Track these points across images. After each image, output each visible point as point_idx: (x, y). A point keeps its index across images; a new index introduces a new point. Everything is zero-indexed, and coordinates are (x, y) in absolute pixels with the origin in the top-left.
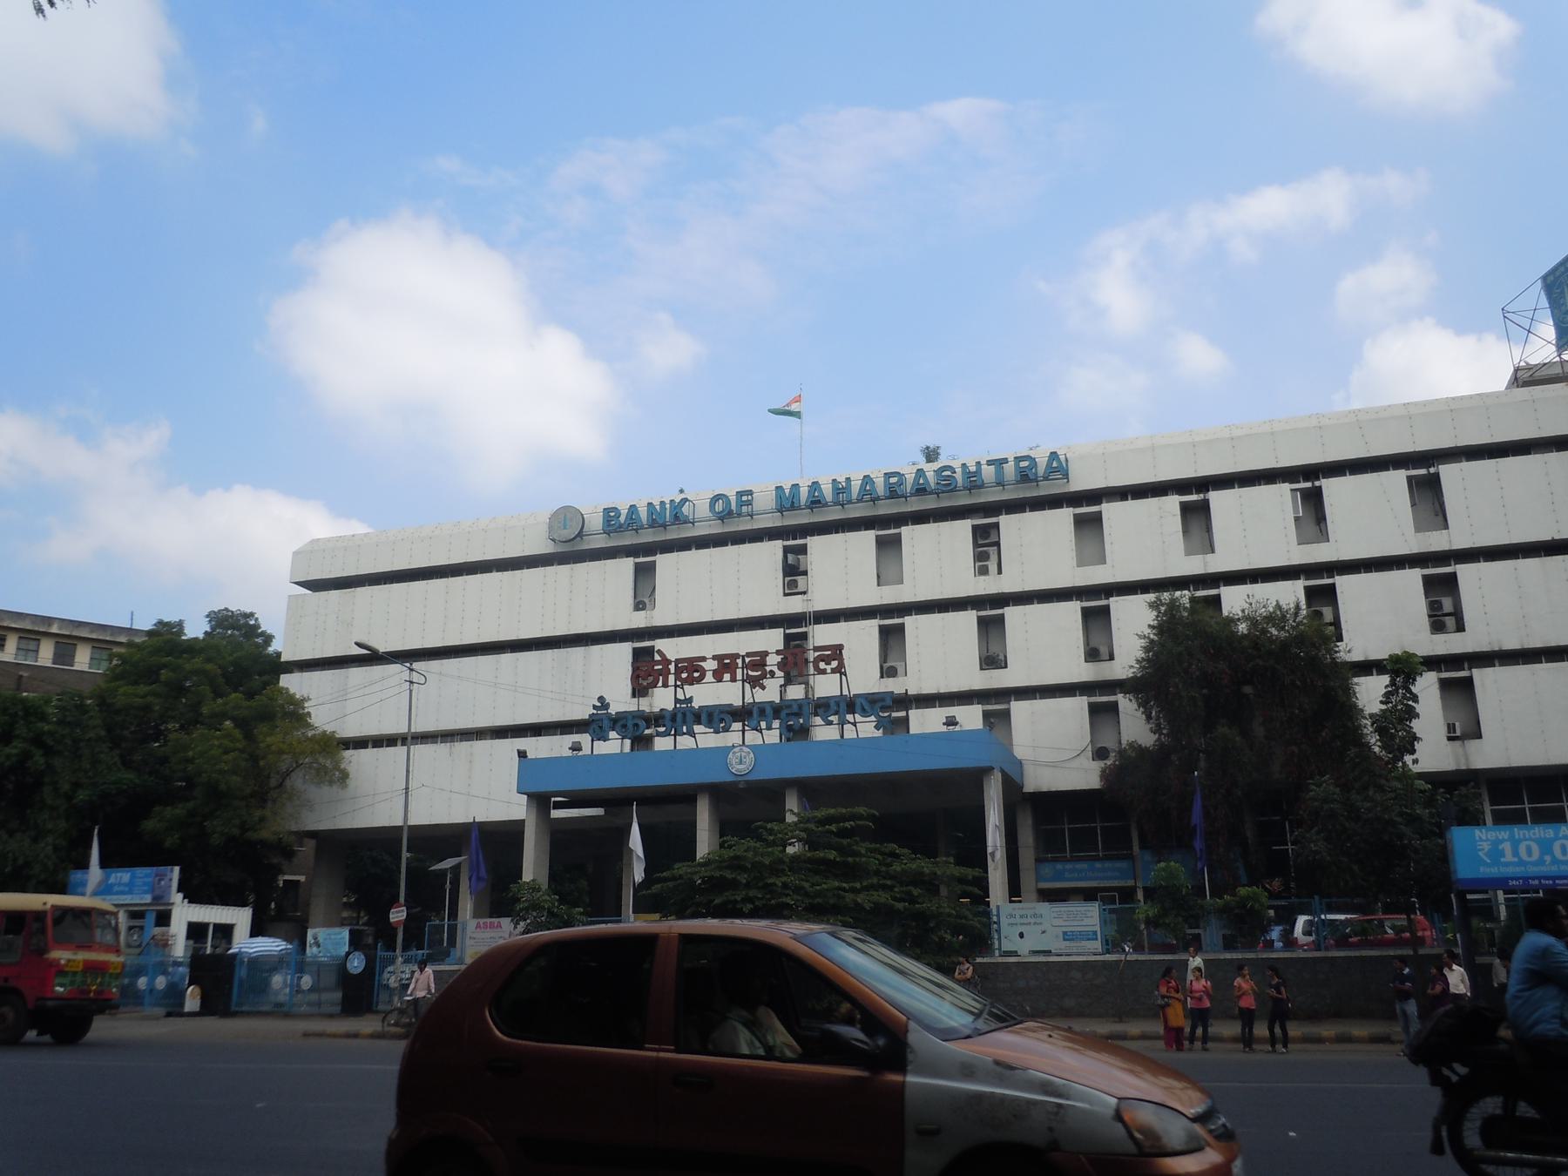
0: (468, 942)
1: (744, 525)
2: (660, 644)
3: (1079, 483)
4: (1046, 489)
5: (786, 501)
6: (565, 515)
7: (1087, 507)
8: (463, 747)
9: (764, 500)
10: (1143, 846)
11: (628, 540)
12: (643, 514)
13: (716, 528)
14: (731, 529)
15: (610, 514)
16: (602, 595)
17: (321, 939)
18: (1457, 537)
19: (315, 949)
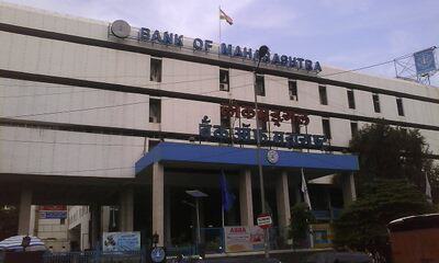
0: (226, 240)
1: (203, 55)
2: (421, 131)
3: (321, 75)
4: (311, 74)
5: (226, 50)
6: (121, 24)
7: (323, 84)
8: (50, 132)
9: (216, 45)
10: (332, 204)
11: (148, 46)
12: (234, 49)
13: (190, 53)
14: (199, 54)
15: (145, 31)
16: (135, 68)
17: (115, 239)
18: (164, 87)
19: (110, 247)
